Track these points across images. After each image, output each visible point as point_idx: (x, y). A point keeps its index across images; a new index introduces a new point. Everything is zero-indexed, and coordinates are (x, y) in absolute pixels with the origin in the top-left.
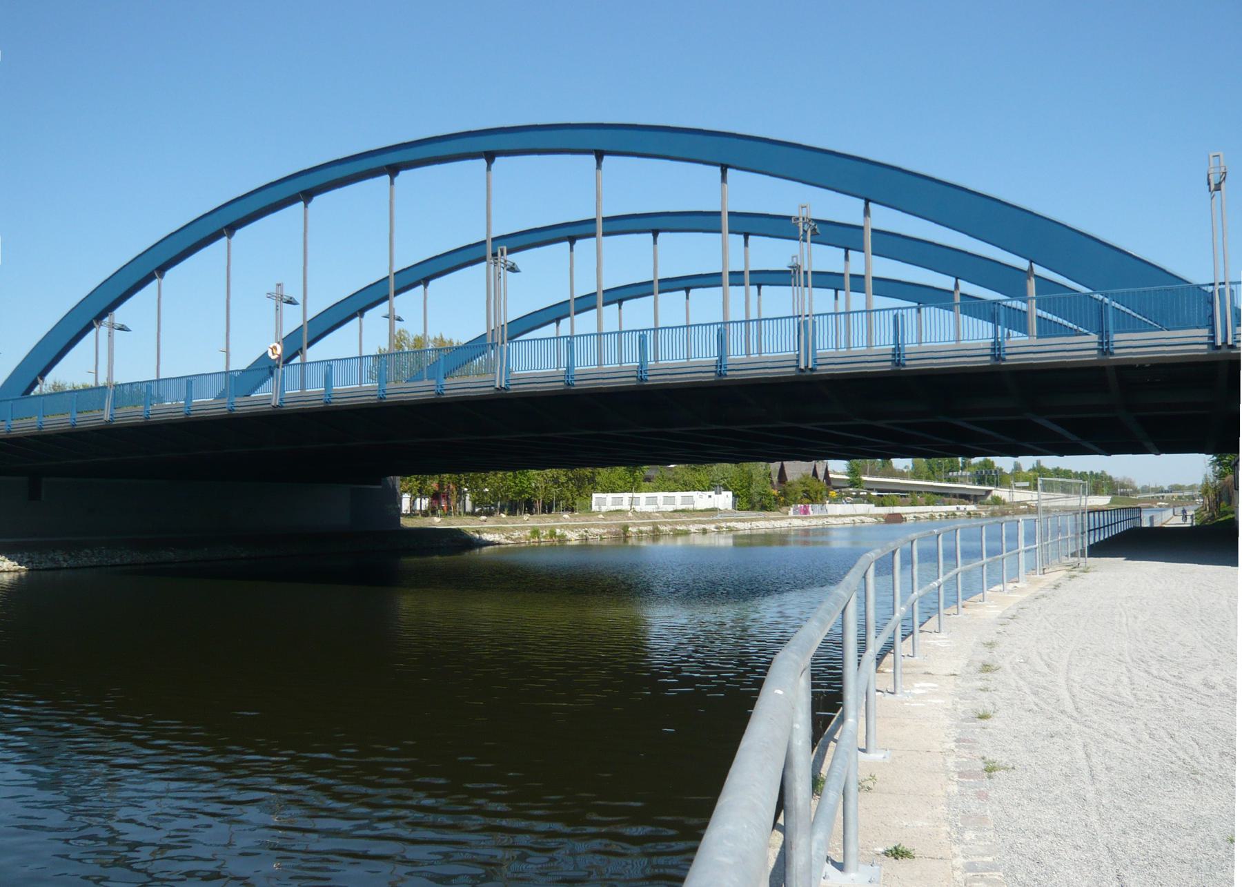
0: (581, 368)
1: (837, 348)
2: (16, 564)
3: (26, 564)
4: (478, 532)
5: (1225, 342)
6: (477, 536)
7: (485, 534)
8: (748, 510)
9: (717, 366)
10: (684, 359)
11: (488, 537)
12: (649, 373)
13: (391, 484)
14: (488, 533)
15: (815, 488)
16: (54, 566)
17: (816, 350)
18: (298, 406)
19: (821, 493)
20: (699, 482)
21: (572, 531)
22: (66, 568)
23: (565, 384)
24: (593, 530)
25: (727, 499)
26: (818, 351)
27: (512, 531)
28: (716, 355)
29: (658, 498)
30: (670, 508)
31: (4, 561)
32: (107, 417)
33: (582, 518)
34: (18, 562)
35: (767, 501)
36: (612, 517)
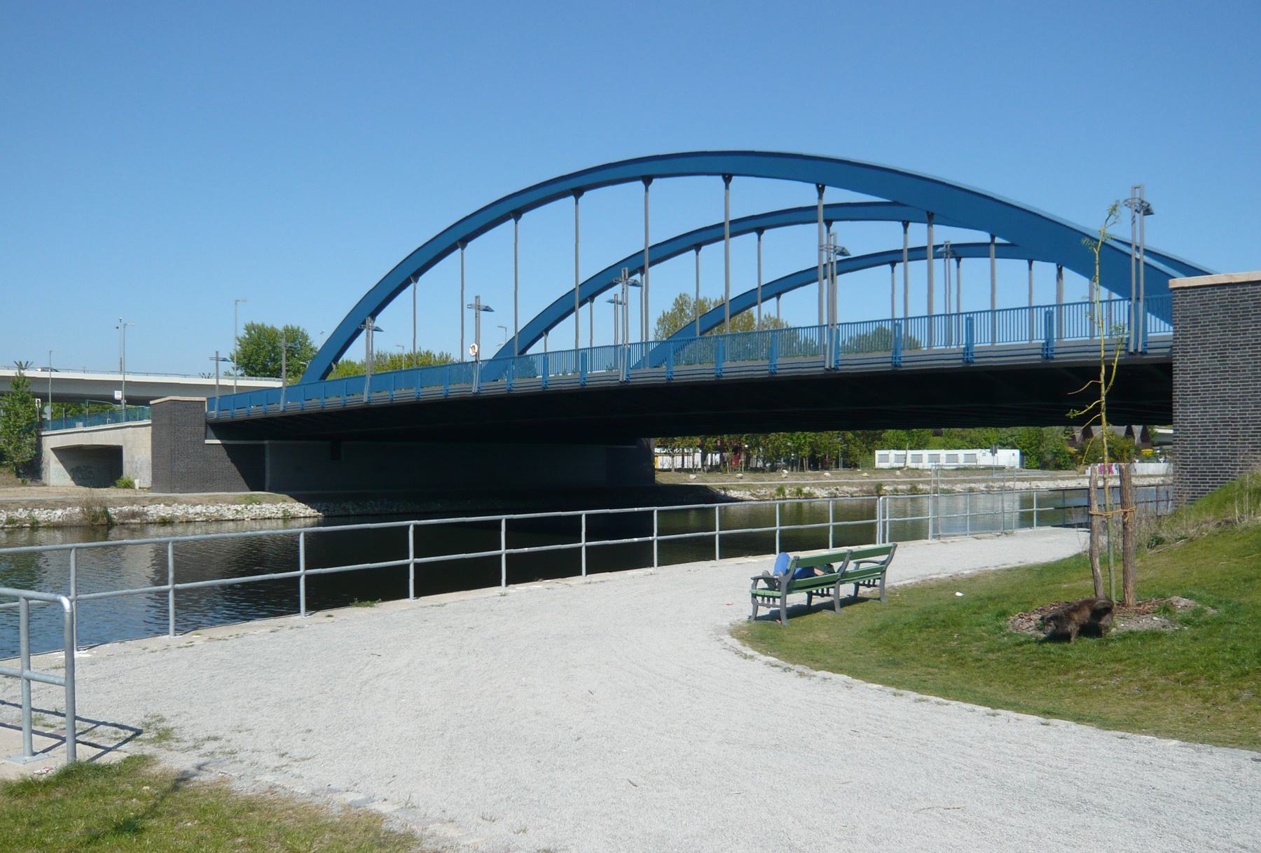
0: (1155, 334)
1: (958, 345)
2: (316, 511)
3: (323, 512)
4: (724, 489)
5: (1136, 350)
6: (723, 492)
7: (731, 491)
8: (1038, 469)
9: (1043, 349)
10: (1086, 336)
11: (733, 494)
12: (1056, 351)
13: (645, 444)
14: (734, 490)
15: (1120, 446)
16: (344, 513)
17: (1147, 333)
18: (936, 364)
19: (1128, 451)
20: (985, 439)
21: (823, 489)
22: (353, 515)
23: (893, 365)
24: (845, 488)
25: (1013, 457)
26: (1149, 335)
27: (760, 488)
28: (1043, 338)
29: (941, 456)
30: (953, 465)
31: (307, 509)
32: (475, 390)
33: (844, 476)
34: (317, 510)
35: (1062, 460)
36: (878, 475)
